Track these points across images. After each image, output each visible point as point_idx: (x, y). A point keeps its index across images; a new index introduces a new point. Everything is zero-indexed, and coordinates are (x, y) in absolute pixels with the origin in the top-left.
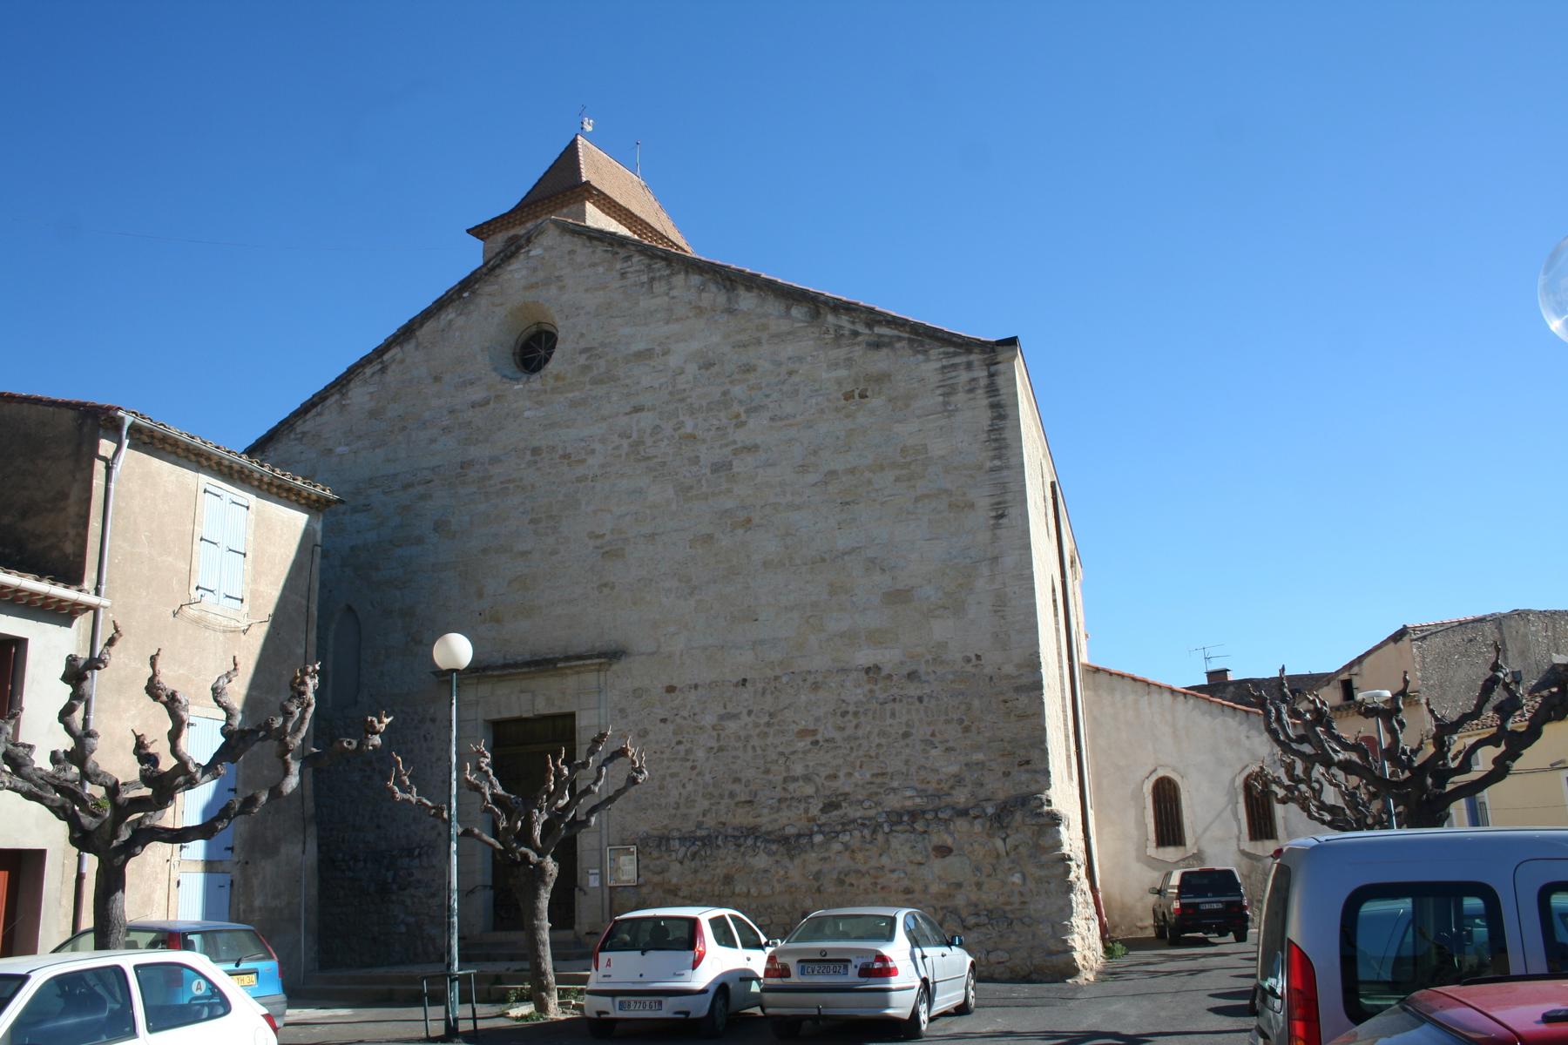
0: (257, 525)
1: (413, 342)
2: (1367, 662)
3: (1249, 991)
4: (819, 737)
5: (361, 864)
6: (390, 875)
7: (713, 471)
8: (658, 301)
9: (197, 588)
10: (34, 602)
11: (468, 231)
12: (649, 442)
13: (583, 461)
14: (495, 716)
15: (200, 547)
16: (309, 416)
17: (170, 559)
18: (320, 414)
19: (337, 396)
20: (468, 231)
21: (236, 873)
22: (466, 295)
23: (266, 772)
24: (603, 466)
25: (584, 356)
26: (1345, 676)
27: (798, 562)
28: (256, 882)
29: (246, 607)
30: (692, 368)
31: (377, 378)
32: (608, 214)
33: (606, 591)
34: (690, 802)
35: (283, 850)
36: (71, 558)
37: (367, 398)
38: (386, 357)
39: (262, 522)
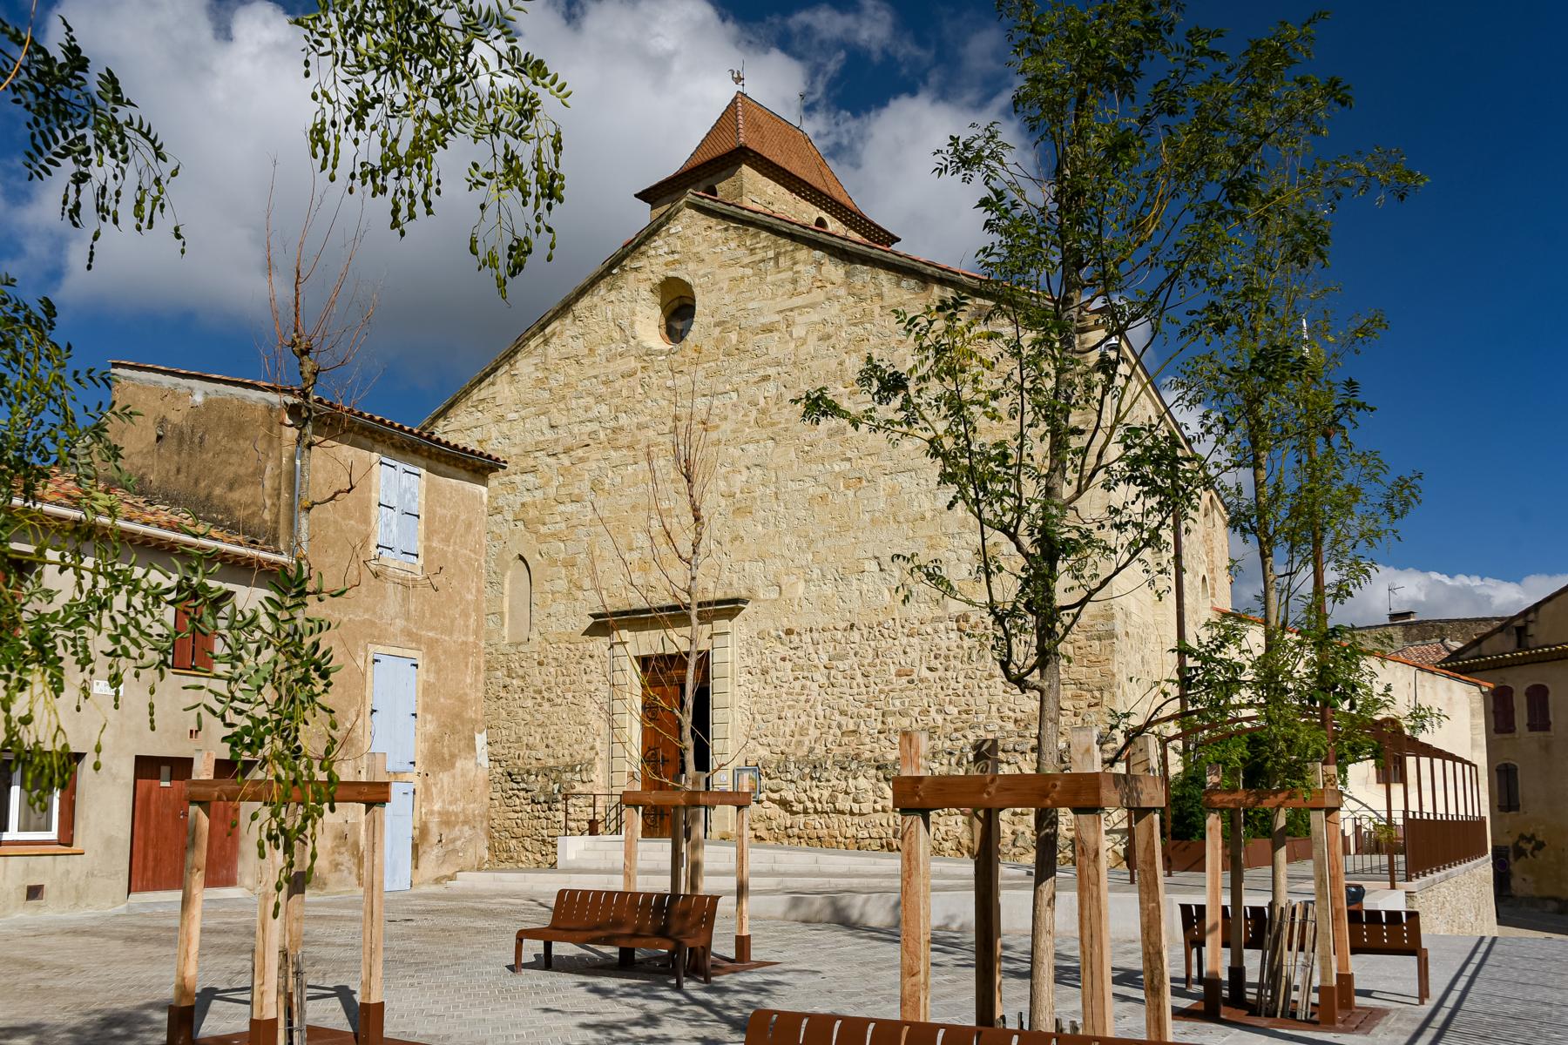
0: (428, 491)
1: (571, 315)
2: (1542, 610)
3: (136, 891)
4: (914, 677)
5: (533, 777)
6: (556, 787)
7: (830, 436)
8: (783, 276)
9: (378, 546)
10: (238, 562)
11: (636, 196)
12: (774, 410)
13: (717, 427)
14: (644, 653)
15: (375, 511)
16: (483, 385)
17: (352, 522)
18: (493, 384)
19: (507, 367)
20: (636, 196)
21: (418, 783)
22: (614, 271)
23: (442, 700)
24: (734, 431)
25: (718, 329)
26: (1520, 623)
27: (902, 520)
28: (434, 790)
29: (420, 562)
30: (812, 340)
31: (540, 350)
32: (764, 175)
33: (737, 543)
34: (803, 732)
35: (459, 764)
36: (905, 71)
37: (533, 368)
38: (548, 330)
39: (430, 489)
